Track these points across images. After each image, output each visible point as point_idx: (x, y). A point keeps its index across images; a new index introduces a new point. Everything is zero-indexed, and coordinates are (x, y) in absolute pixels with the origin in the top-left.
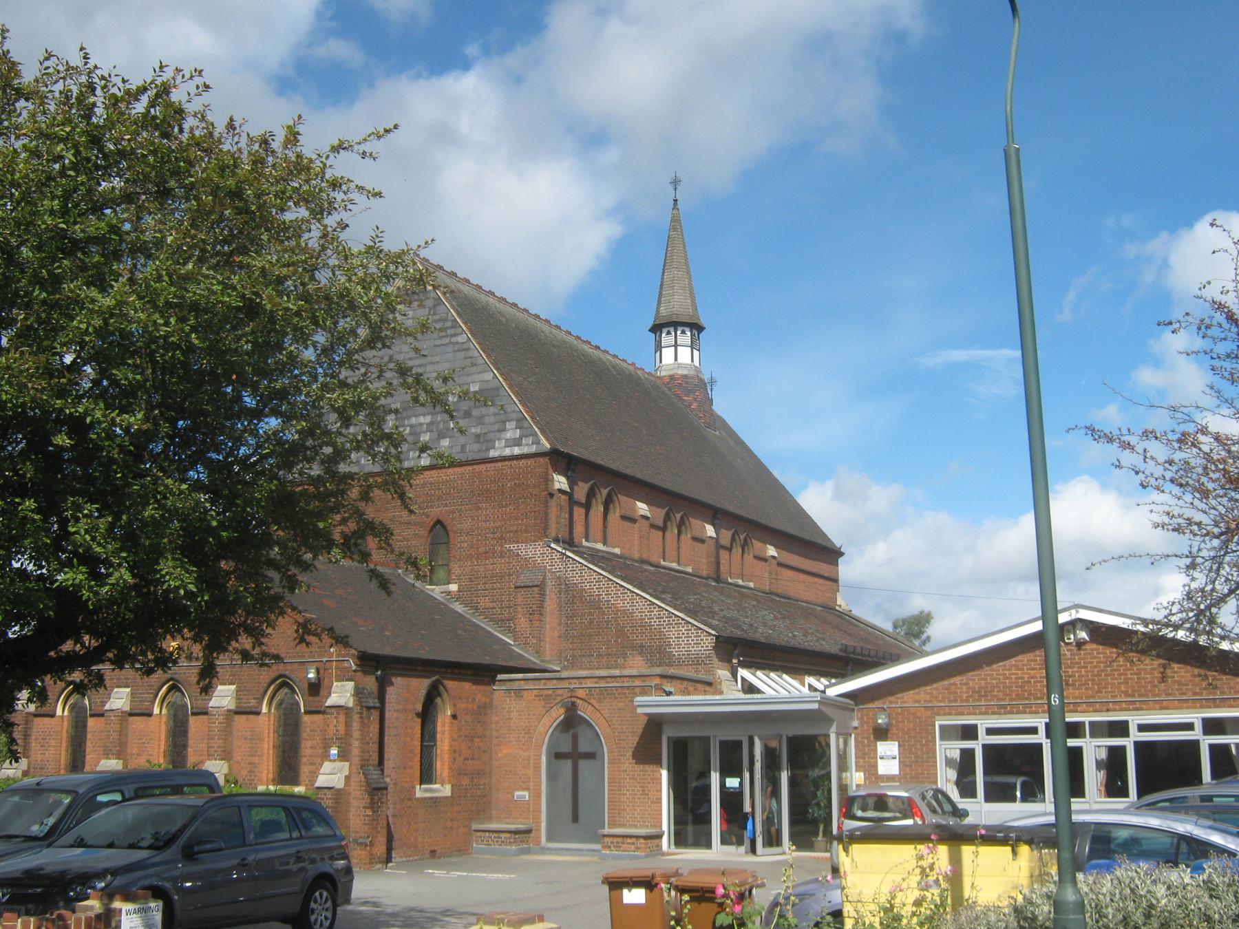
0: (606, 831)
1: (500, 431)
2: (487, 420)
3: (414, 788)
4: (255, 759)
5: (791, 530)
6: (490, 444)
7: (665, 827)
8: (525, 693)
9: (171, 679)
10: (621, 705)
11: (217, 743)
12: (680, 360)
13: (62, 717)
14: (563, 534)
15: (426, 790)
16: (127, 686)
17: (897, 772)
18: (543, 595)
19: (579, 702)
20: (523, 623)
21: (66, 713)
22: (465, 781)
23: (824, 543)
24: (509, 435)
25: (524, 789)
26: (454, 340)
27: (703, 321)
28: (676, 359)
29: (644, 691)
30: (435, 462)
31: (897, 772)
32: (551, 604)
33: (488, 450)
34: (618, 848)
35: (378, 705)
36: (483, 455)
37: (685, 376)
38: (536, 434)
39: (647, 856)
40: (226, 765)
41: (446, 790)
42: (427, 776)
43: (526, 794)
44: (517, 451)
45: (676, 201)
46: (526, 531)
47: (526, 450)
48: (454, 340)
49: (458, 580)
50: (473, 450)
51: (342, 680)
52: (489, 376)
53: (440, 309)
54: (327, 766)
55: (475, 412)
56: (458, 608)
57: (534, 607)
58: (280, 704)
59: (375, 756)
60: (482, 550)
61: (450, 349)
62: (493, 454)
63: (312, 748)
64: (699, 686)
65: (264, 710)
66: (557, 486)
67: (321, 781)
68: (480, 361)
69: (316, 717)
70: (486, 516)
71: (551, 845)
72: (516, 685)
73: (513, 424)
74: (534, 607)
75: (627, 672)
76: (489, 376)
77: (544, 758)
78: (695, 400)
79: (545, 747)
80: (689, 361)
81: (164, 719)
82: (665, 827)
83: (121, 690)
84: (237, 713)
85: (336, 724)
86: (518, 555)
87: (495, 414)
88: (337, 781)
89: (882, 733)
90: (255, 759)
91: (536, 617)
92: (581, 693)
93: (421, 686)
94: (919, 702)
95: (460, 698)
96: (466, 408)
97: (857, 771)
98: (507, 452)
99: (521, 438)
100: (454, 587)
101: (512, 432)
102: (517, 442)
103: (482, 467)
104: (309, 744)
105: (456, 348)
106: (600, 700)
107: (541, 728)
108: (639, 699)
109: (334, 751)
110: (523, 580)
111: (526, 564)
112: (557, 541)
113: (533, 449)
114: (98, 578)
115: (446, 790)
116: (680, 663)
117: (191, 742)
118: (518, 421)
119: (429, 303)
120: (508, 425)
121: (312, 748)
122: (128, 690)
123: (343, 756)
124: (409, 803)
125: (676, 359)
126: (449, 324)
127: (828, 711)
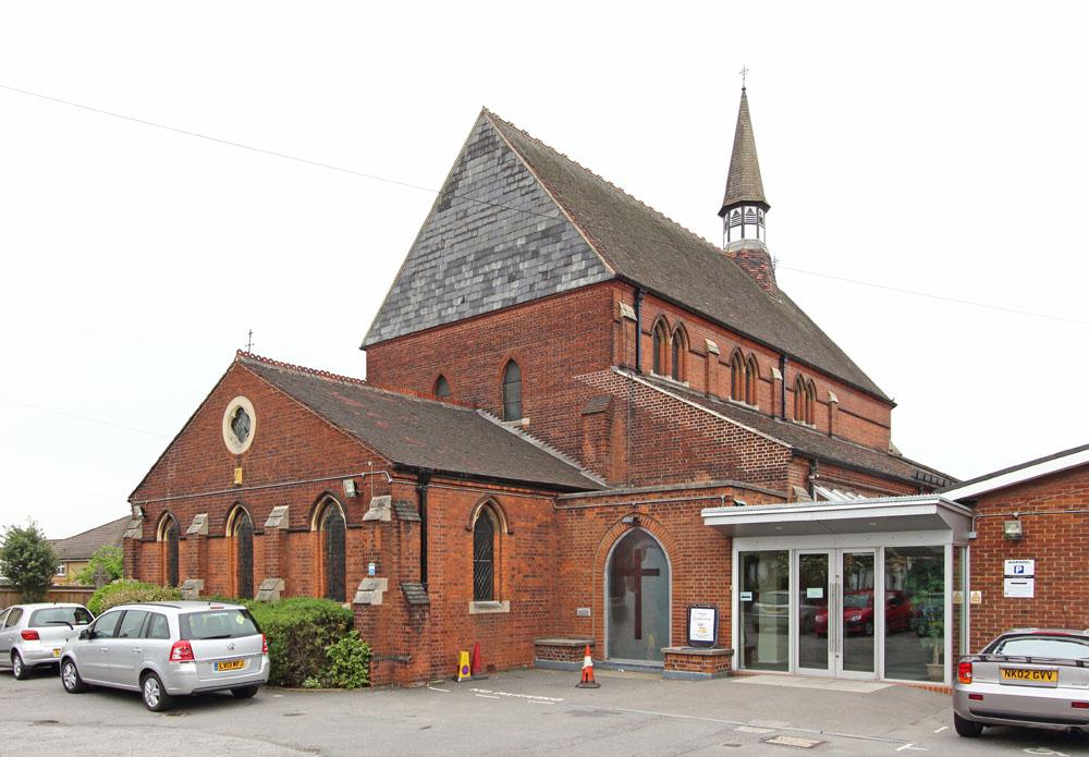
0: (671, 649)
1: (566, 265)
2: (554, 257)
3: (466, 604)
4: (307, 577)
5: (851, 380)
6: (556, 278)
7: (735, 646)
8: (587, 512)
9: (237, 503)
10: (685, 520)
11: (274, 561)
12: (746, 237)
13: (162, 543)
14: (630, 361)
15: (481, 607)
16: (205, 512)
17: (1032, 596)
18: (610, 421)
19: (642, 518)
20: (589, 451)
21: (165, 539)
22: (526, 598)
23: (876, 392)
24: (574, 268)
25: (586, 606)
26: (521, 184)
27: (769, 201)
28: (743, 236)
29: (713, 503)
30: (506, 305)
31: (1032, 596)
32: (619, 422)
33: (555, 285)
34: (682, 667)
35: (419, 519)
36: (550, 292)
37: (751, 251)
38: (602, 263)
39: (713, 677)
40: (282, 582)
41: (506, 607)
42: (483, 591)
43: (588, 609)
44: (582, 282)
45: (744, 89)
46: (593, 361)
47: (591, 280)
48: (521, 184)
49: (530, 415)
50: (541, 288)
51: (379, 495)
52: (554, 214)
53: (508, 157)
54: (365, 583)
55: (543, 251)
56: (528, 439)
57: (601, 433)
58: (328, 522)
59: (417, 571)
60: (551, 383)
61: (518, 193)
62: (560, 288)
63: (355, 564)
64: (773, 499)
65: (314, 528)
66: (624, 313)
67: (359, 597)
68: (546, 200)
69: (357, 532)
70: (554, 350)
71: (612, 660)
72: (578, 504)
73: (579, 257)
74: (601, 433)
75: (693, 485)
76: (554, 214)
77: (606, 575)
78: (760, 271)
79: (607, 564)
80: (755, 237)
81: (236, 541)
82: (735, 646)
83: (201, 516)
84: (289, 532)
85: (373, 539)
86: (585, 385)
87: (561, 250)
88: (377, 599)
89: (1016, 547)
90: (307, 577)
91: (603, 442)
92: (644, 509)
93: (470, 502)
94: (1066, 507)
95: (519, 517)
96: (534, 248)
97: (971, 589)
98: (574, 285)
99: (586, 269)
100: (526, 421)
101: (578, 264)
102: (583, 274)
103: (549, 304)
104: (352, 560)
105: (524, 192)
106: (664, 516)
107: (603, 546)
108: (706, 512)
109: (372, 567)
110: (590, 408)
111: (595, 393)
112: (622, 367)
113: (599, 278)
114: (547, 561)
115: (506, 607)
116: (751, 477)
117: (255, 561)
118: (583, 252)
119: (499, 153)
120: (574, 258)
121: (355, 564)
122: (206, 515)
123: (379, 572)
124: (461, 620)
125: (743, 236)
126: (516, 170)
127: (944, 516)
